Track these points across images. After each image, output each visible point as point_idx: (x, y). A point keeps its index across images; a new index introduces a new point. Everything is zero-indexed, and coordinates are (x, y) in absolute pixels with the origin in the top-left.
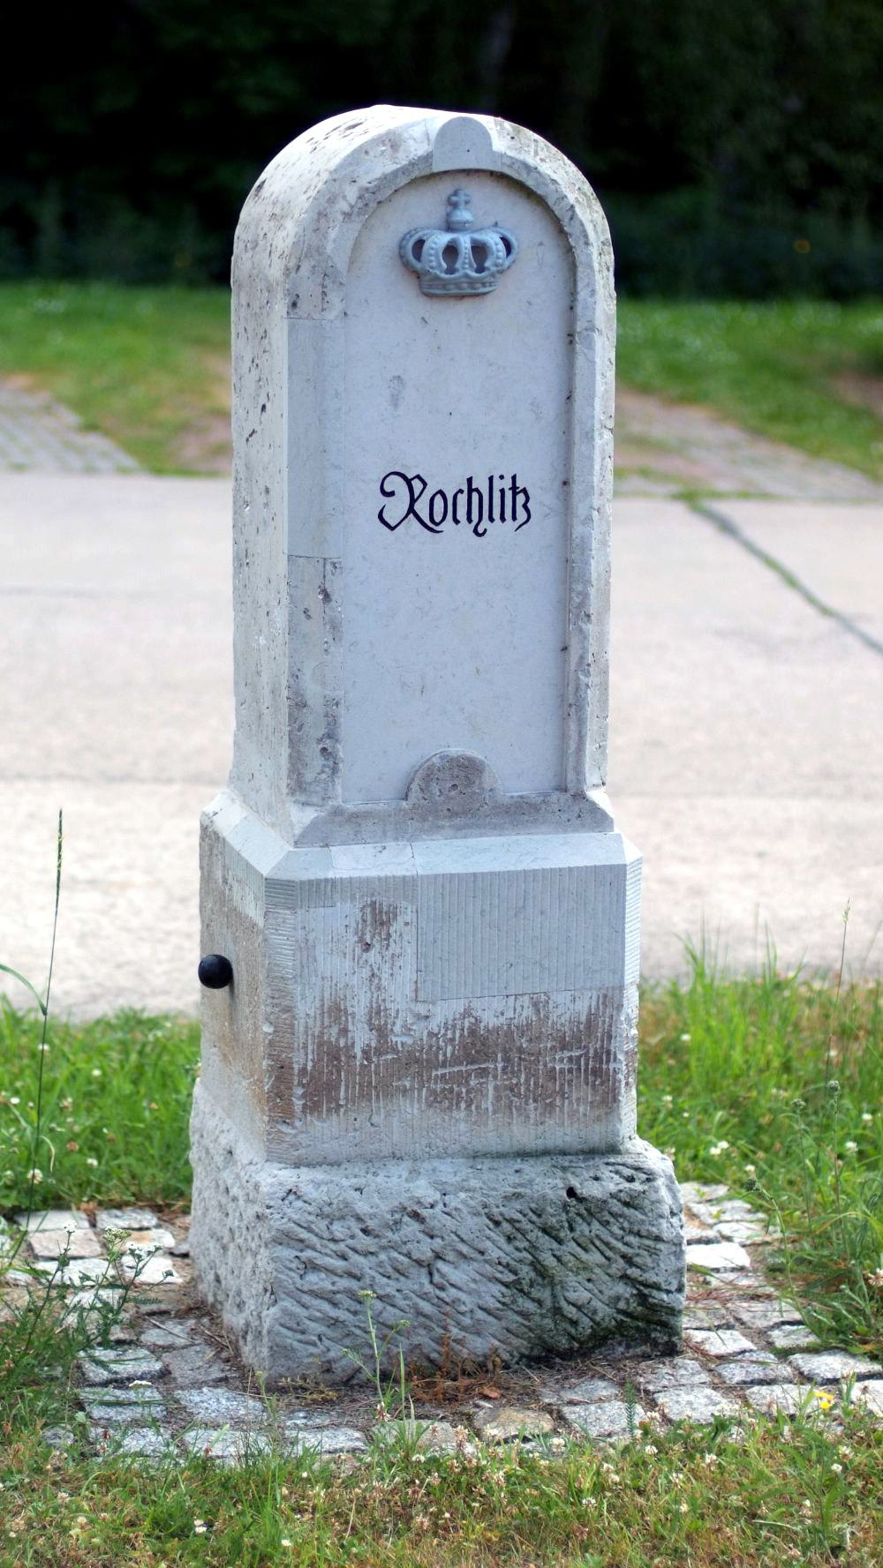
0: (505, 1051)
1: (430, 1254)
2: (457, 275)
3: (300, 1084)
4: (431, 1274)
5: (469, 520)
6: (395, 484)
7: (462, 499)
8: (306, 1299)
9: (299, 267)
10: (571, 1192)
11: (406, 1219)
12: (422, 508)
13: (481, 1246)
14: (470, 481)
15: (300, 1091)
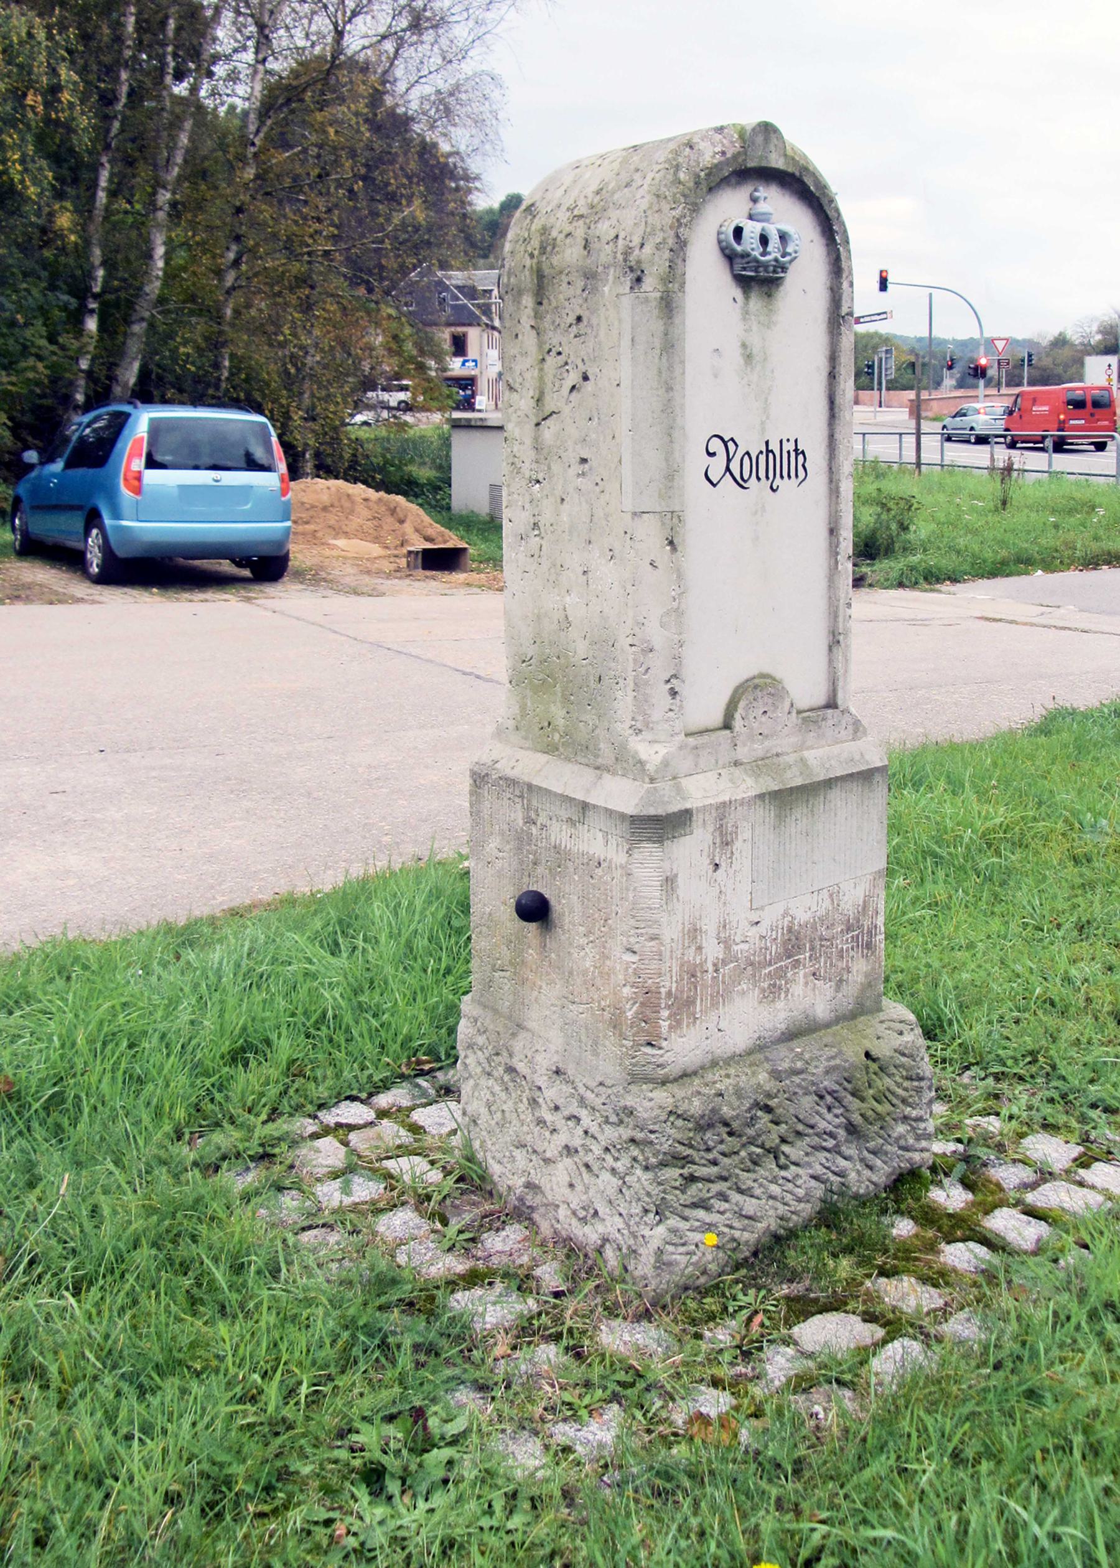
0: (811, 941)
1: (777, 1141)
2: (768, 258)
3: (668, 1007)
4: (776, 1157)
5: (767, 478)
6: (716, 446)
7: (762, 458)
8: (687, 1212)
9: (642, 245)
10: (868, 1055)
11: (760, 1113)
12: (735, 467)
13: (812, 1122)
14: (767, 443)
15: (665, 1013)
